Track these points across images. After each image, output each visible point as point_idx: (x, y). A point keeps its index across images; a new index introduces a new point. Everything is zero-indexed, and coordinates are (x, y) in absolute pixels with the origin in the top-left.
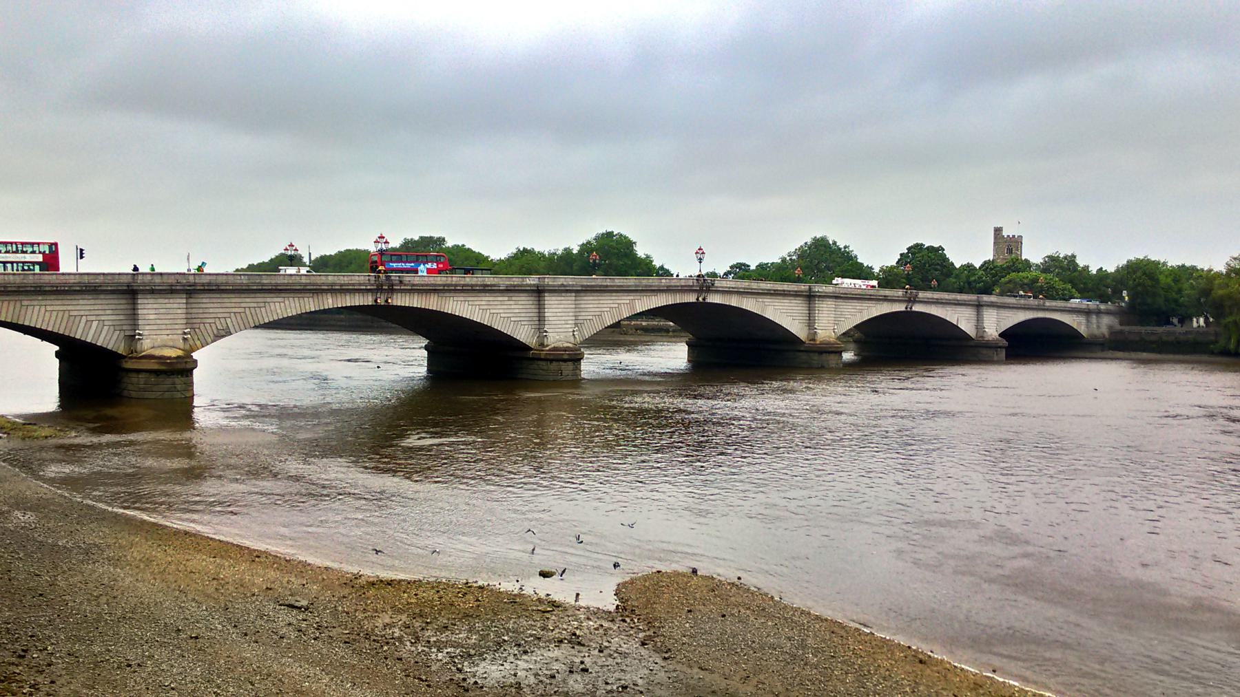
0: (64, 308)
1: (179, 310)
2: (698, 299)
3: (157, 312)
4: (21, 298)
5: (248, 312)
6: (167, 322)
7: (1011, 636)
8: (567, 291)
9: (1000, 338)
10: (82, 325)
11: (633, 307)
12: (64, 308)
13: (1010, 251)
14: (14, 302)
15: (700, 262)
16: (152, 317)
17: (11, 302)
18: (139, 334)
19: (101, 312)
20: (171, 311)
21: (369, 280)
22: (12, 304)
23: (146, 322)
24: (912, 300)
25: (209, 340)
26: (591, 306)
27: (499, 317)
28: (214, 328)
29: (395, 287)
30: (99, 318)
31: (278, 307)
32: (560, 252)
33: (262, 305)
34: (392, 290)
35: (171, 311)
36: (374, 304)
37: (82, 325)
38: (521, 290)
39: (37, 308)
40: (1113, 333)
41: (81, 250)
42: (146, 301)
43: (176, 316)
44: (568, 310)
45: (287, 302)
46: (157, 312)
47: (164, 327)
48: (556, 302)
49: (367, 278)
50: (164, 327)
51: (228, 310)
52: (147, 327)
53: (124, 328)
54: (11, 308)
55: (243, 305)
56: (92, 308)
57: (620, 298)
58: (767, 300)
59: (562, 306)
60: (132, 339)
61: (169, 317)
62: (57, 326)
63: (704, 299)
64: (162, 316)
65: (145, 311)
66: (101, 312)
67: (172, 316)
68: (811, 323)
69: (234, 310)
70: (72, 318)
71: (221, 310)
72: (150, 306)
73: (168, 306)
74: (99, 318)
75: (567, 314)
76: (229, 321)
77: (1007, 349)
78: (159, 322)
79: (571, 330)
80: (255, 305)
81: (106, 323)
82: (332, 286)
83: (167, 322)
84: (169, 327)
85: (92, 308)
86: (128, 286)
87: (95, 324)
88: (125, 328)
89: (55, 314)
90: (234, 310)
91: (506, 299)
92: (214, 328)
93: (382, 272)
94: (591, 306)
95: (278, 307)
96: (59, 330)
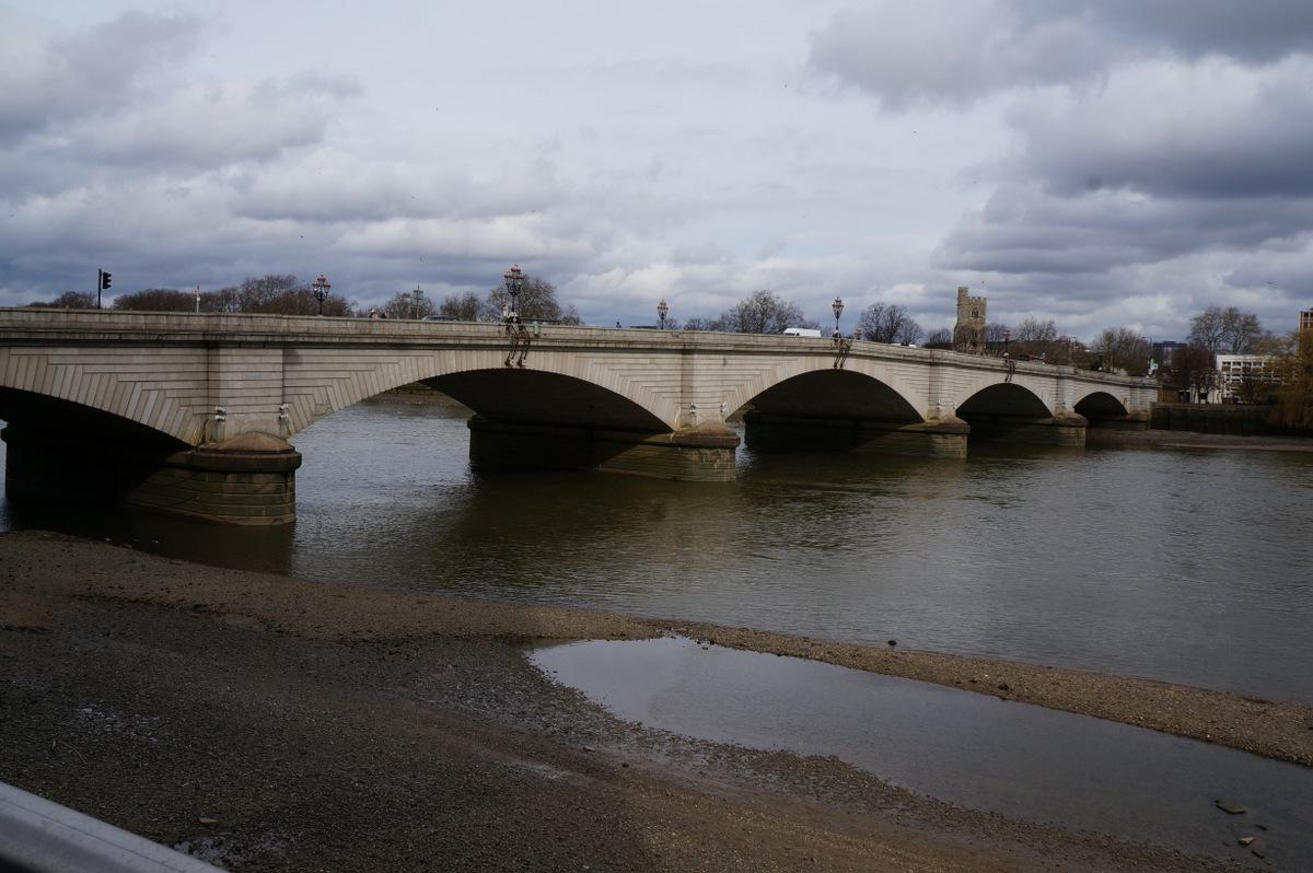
0: (111, 369)
1: (273, 374)
2: (507, 363)
3: (245, 376)
4: (10, 347)
5: (354, 379)
6: (257, 393)
7: (820, 851)
8: (265, 345)
9: (1077, 416)
10: (136, 396)
11: (775, 375)
12: (111, 369)
13: (976, 314)
14: (26, 358)
15: (838, 317)
16: (238, 385)
17: (23, 357)
18: (220, 413)
19: (162, 377)
20: (263, 376)
21: (499, 332)
22: (34, 360)
23: (230, 393)
24: (1012, 371)
25: (305, 422)
26: (734, 373)
27: (113, 382)
28: (311, 401)
29: (532, 343)
30: (159, 386)
31: (391, 371)
32: (460, 300)
33: (372, 367)
34: (527, 348)
35: (263, 376)
36: (505, 367)
37: (136, 396)
38: (566, 347)
39: (71, 369)
40: (1156, 409)
41: (106, 275)
42: (229, 360)
43: (270, 384)
44: (716, 378)
45: (402, 363)
46: (245, 376)
47: (253, 401)
48: (704, 367)
49: (497, 328)
50: (253, 401)
51: (331, 375)
52: (231, 402)
53: (193, 403)
54: (33, 366)
55: (349, 367)
56: (150, 368)
57: (125, 360)
58: (895, 366)
59: (710, 373)
60: (209, 420)
61: (259, 384)
62: (100, 398)
63: (519, 363)
64: (253, 384)
65: (229, 376)
66: (162, 377)
67: (263, 384)
68: (932, 397)
69: (338, 375)
70: (121, 386)
71: (321, 375)
72: (235, 368)
73: (259, 367)
74: (159, 386)
75: (714, 384)
76: (330, 390)
77: (1086, 422)
78: (246, 393)
79: (719, 405)
80: (363, 367)
81: (169, 394)
82: (105, 334)
83: (257, 393)
84: (260, 401)
85: (150, 368)
86: (204, 335)
87: (153, 395)
88: (194, 401)
89: (97, 377)
90: (338, 375)
91: (648, 361)
92: (311, 401)
93: (515, 320)
94: (734, 373)
95: (391, 371)
96: (118, 409)
